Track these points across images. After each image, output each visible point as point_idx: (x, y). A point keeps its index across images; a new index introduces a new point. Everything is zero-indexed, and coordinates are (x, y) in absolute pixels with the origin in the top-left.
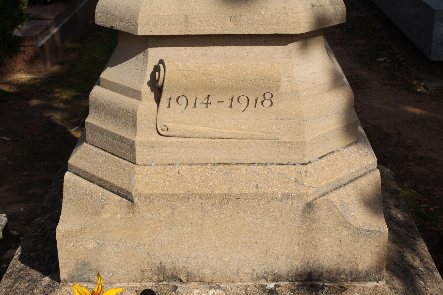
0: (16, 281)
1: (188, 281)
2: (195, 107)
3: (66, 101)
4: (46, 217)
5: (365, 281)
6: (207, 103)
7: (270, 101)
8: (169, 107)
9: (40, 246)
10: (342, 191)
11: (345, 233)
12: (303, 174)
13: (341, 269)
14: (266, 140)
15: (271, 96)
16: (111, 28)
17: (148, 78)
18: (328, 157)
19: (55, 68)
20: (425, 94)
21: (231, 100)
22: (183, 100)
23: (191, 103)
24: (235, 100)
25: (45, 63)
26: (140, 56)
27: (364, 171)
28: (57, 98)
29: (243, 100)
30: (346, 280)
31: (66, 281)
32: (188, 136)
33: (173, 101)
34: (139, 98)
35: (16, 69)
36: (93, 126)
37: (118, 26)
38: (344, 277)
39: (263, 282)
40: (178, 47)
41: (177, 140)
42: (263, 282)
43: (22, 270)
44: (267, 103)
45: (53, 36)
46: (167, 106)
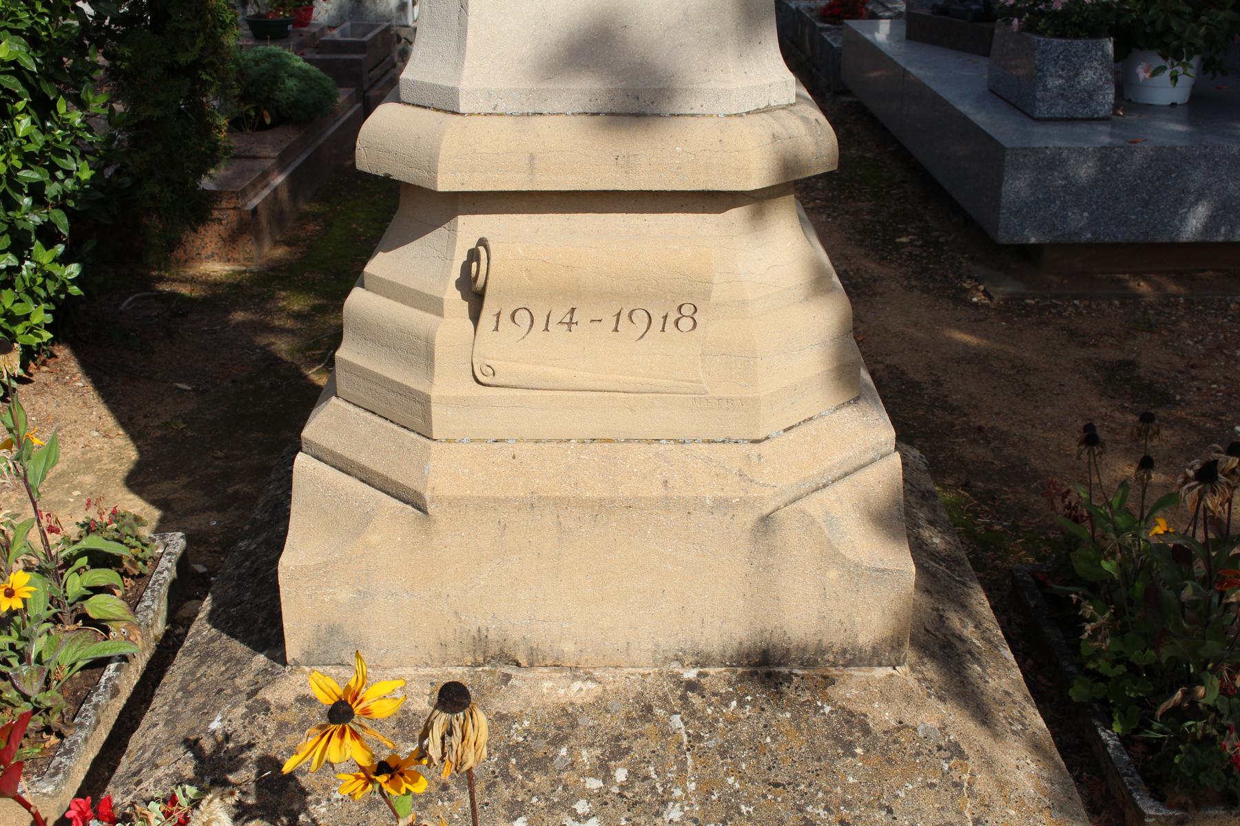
1: (531, 665)
2: (547, 329)
3: (298, 316)
4: (260, 539)
5: (870, 665)
6: (571, 323)
7: (691, 320)
8: (496, 329)
10: (827, 495)
11: (833, 574)
12: (755, 460)
13: (825, 643)
14: (682, 396)
15: (693, 311)
16: (387, 179)
17: (456, 274)
18: (803, 429)
19: (280, 252)
21: (615, 318)
22: (523, 317)
23: (540, 322)
24: (624, 317)
25: (258, 241)
26: (441, 232)
27: (871, 455)
28: (282, 310)
29: (640, 317)
30: (834, 665)
31: (297, 664)
32: (534, 386)
33: (505, 318)
34: (439, 312)
37: (400, 173)
38: (830, 657)
39: (676, 667)
40: (514, 215)
41: (512, 394)
42: (676, 667)
44: (686, 324)
45: (275, 191)
46: (493, 328)
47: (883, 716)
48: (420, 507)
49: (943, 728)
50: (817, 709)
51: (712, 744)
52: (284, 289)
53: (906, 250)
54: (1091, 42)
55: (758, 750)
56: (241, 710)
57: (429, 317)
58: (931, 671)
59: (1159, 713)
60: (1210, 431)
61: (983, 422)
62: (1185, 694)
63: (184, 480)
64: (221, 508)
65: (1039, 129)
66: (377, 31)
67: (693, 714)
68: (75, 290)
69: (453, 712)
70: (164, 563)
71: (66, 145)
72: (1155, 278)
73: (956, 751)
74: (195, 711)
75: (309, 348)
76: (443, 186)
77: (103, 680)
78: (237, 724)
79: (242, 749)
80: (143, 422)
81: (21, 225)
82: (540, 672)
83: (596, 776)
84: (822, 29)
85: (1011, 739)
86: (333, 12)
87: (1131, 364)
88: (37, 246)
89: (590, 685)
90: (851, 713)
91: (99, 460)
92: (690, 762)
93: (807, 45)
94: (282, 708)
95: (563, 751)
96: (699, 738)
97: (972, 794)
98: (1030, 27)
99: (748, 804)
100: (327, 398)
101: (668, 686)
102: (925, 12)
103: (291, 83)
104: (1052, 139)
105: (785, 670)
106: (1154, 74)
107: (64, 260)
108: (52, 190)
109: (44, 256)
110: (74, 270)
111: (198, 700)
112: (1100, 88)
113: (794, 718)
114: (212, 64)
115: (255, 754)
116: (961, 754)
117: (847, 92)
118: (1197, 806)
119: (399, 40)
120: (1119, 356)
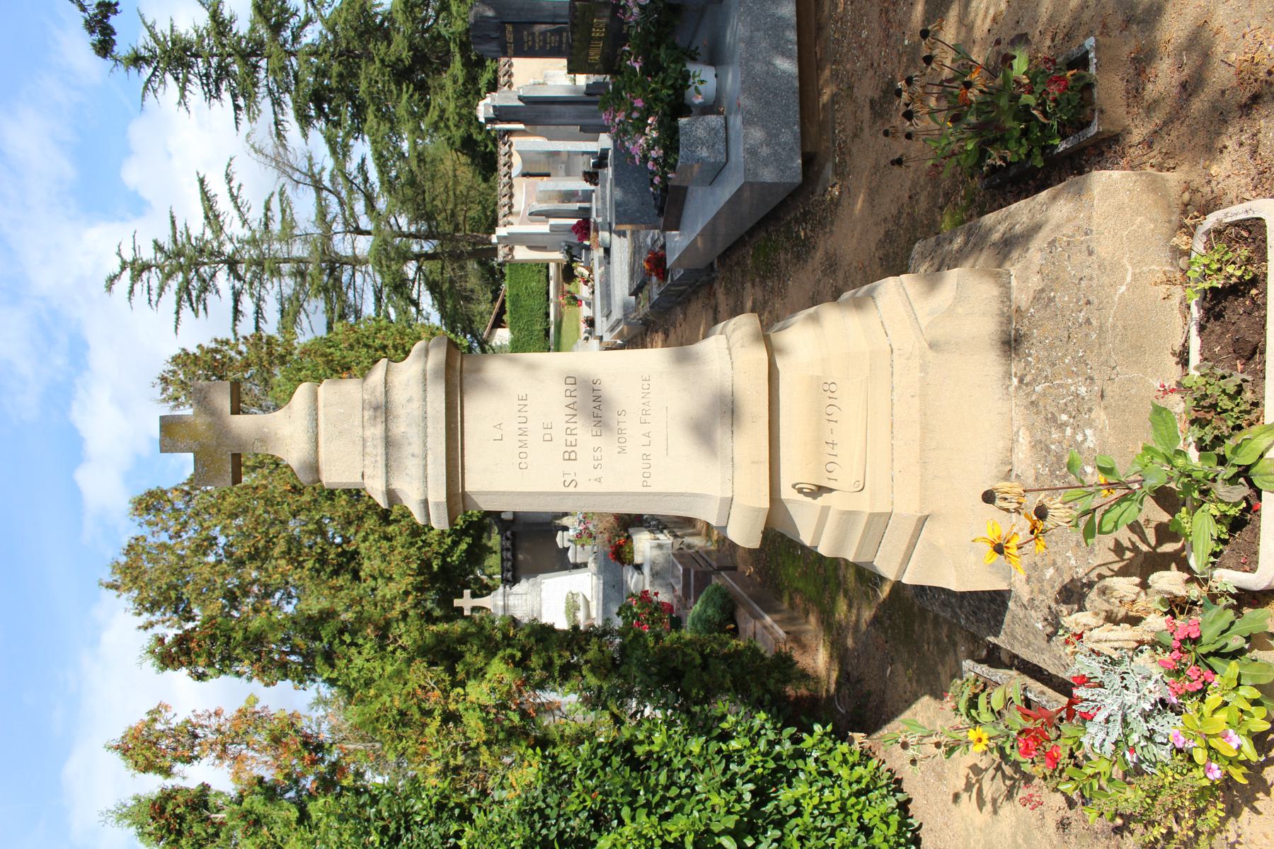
0: (1015, 638)
1: (1011, 463)
3: (850, 606)
4: (959, 612)
5: (1010, 288)
9: (985, 616)
10: (919, 314)
11: (960, 310)
12: (901, 352)
13: (999, 312)
16: (763, 533)
17: (809, 499)
18: (886, 326)
19: (813, 619)
20: (841, 186)
22: (830, 467)
23: (832, 459)
24: (830, 418)
25: (805, 632)
26: (789, 506)
27: (901, 290)
28: (846, 616)
29: (830, 410)
30: (1010, 307)
31: (1010, 584)
33: (830, 476)
34: (829, 508)
35: (812, 665)
36: (856, 554)
37: (761, 526)
38: (1006, 309)
39: (1012, 389)
42: (1012, 389)
43: (1006, 633)
44: (833, 387)
45: (775, 621)
47: (1035, 282)
48: (926, 518)
49: (1041, 250)
50: (1032, 316)
51: (1049, 370)
52: (834, 615)
53: (809, 233)
54: (681, 132)
55: (1052, 347)
56: (1033, 612)
57: (831, 512)
58: (1015, 254)
59: (1046, 122)
60: (908, 60)
61: (907, 195)
62: (1034, 109)
63: (940, 668)
64: (955, 644)
65: (733, 158)
66: (676, 561)
67: (1035, 380)
68: (829, 728)
69: (995, 497)
70: (978, 671)
71: (746, 726)
72: (821, 82)
73: (1052, 243)
74: (1036, 639)
75: (868, 598)
76: (767, 505)
77: (1035, 699)
78: (1039, 615)
79: (1051, 612)
80: (908, 694)
81: (791, 752)
82: (1014, 459)
83: (1065, 430)
84: (672, 280)
85: (1049, 213)
86: (664, 590)
87: (872, 101)
88: (802, 745)
89: (1020, 433)
90: (1034, 298)
91: (929, 718)
92: (1058, 382)
93: (682, 288)
94: (1032, 592)
95: (1053, 447)
96: (1046, 377)
97: (1073, 236)
98: (673, 167)
99: (1078, 351)
100: (875, 567)
101: (1021, 393)
102: (662, 220)
103: (710, 612)
104: (738, 154)
105: (1013, 332)
106: (700, 94)
107: (811, 733)
108: (772, 736)
109: (808, 741)
110: (817, 728)
111: (1031, 637)
112: (708, 124)
113: (1036, 328)
114: (701, 646)
115: (1053, 605)
116: (1054, 241)
117: (712, 264)
118: (1092, 103)
119: (681, 549)
120: (867, 109)
